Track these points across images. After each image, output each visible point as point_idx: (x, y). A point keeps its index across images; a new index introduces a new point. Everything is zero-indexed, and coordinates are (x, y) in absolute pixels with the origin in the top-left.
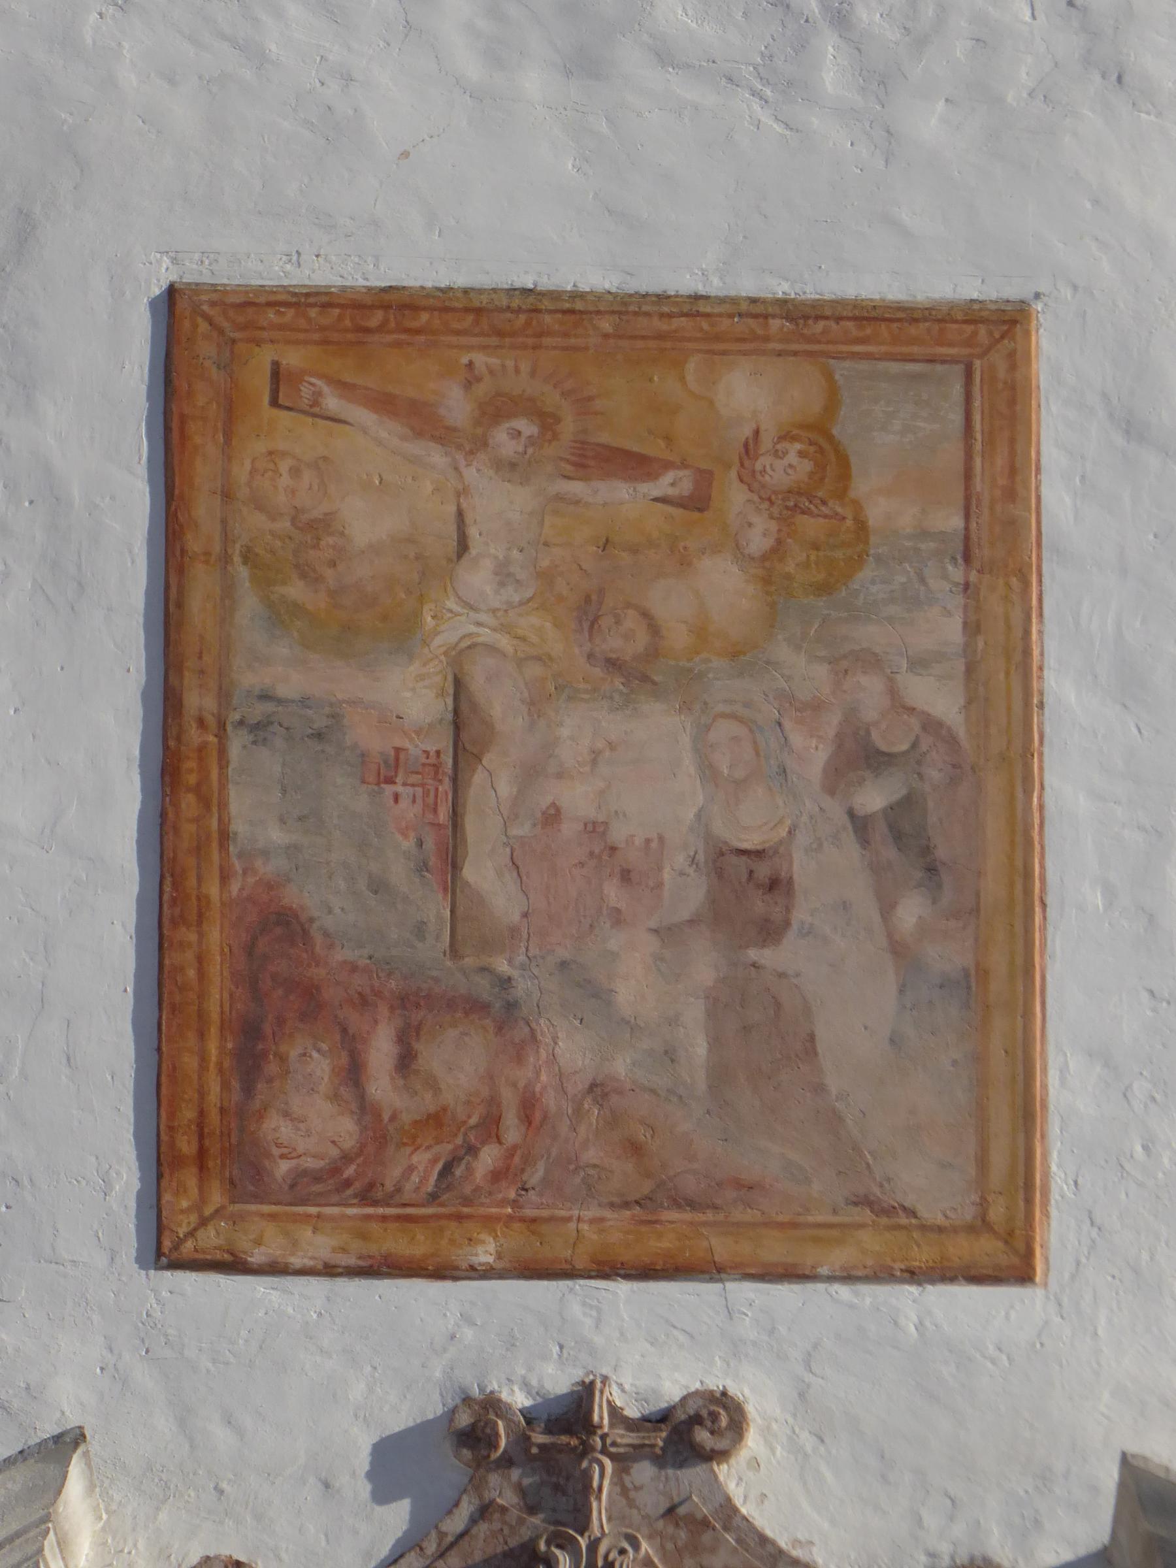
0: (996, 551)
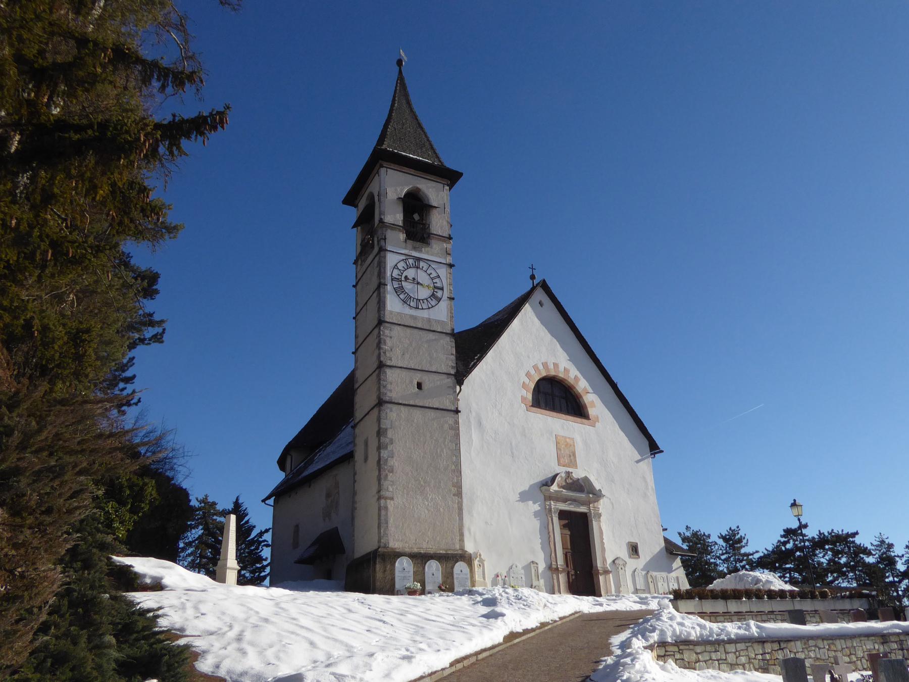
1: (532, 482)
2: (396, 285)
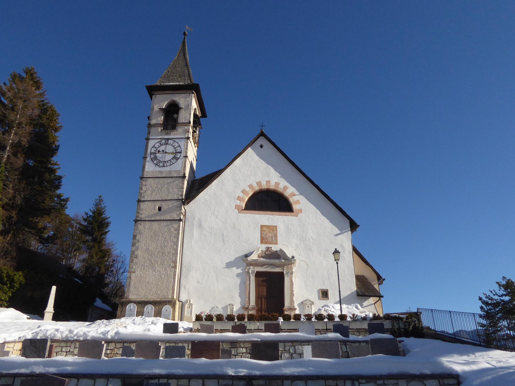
0: (276, 230)
1: (237, 256)
2: (152, 156)
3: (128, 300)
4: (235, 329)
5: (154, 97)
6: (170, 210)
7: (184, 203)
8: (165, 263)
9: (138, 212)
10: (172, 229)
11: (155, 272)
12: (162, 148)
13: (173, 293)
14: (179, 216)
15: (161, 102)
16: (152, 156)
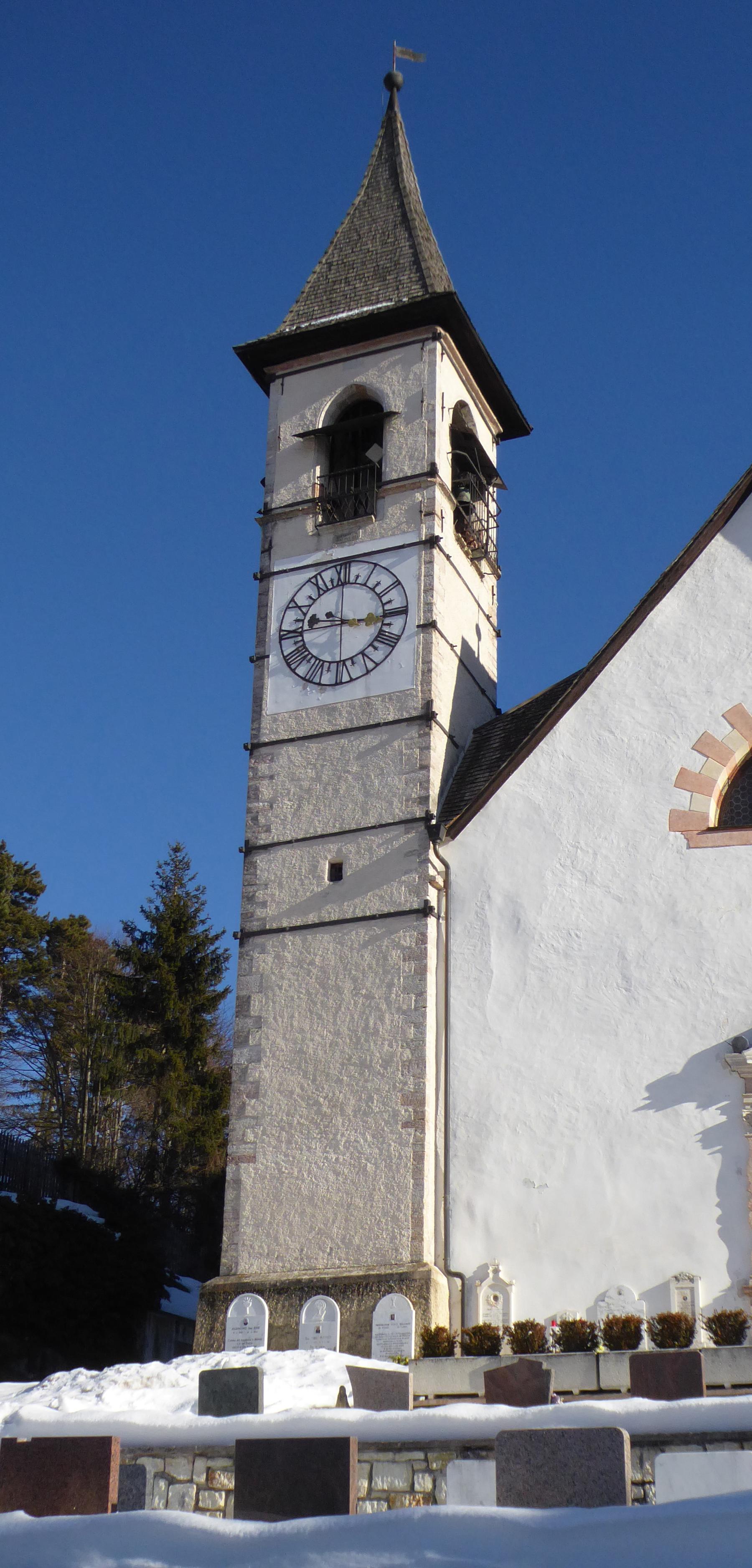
1: (698, 1047)
2: (289, 647)
3: (232, 1280)
4: (497, 1389)
5: (275, 387)
6: (378, 874)
7: (433, 835)
8: (376, 1106)
9: (250, 899)
10: (395, 955)
11: (336, 1149)
12: (327, 603)
13: (418, 1237)
14: (419, 891)
15: (309, 402)
16: (289, 647)
